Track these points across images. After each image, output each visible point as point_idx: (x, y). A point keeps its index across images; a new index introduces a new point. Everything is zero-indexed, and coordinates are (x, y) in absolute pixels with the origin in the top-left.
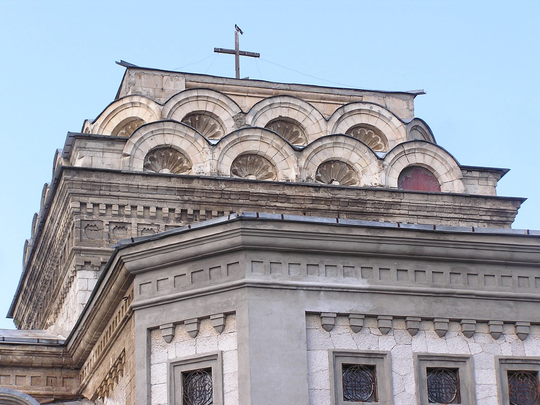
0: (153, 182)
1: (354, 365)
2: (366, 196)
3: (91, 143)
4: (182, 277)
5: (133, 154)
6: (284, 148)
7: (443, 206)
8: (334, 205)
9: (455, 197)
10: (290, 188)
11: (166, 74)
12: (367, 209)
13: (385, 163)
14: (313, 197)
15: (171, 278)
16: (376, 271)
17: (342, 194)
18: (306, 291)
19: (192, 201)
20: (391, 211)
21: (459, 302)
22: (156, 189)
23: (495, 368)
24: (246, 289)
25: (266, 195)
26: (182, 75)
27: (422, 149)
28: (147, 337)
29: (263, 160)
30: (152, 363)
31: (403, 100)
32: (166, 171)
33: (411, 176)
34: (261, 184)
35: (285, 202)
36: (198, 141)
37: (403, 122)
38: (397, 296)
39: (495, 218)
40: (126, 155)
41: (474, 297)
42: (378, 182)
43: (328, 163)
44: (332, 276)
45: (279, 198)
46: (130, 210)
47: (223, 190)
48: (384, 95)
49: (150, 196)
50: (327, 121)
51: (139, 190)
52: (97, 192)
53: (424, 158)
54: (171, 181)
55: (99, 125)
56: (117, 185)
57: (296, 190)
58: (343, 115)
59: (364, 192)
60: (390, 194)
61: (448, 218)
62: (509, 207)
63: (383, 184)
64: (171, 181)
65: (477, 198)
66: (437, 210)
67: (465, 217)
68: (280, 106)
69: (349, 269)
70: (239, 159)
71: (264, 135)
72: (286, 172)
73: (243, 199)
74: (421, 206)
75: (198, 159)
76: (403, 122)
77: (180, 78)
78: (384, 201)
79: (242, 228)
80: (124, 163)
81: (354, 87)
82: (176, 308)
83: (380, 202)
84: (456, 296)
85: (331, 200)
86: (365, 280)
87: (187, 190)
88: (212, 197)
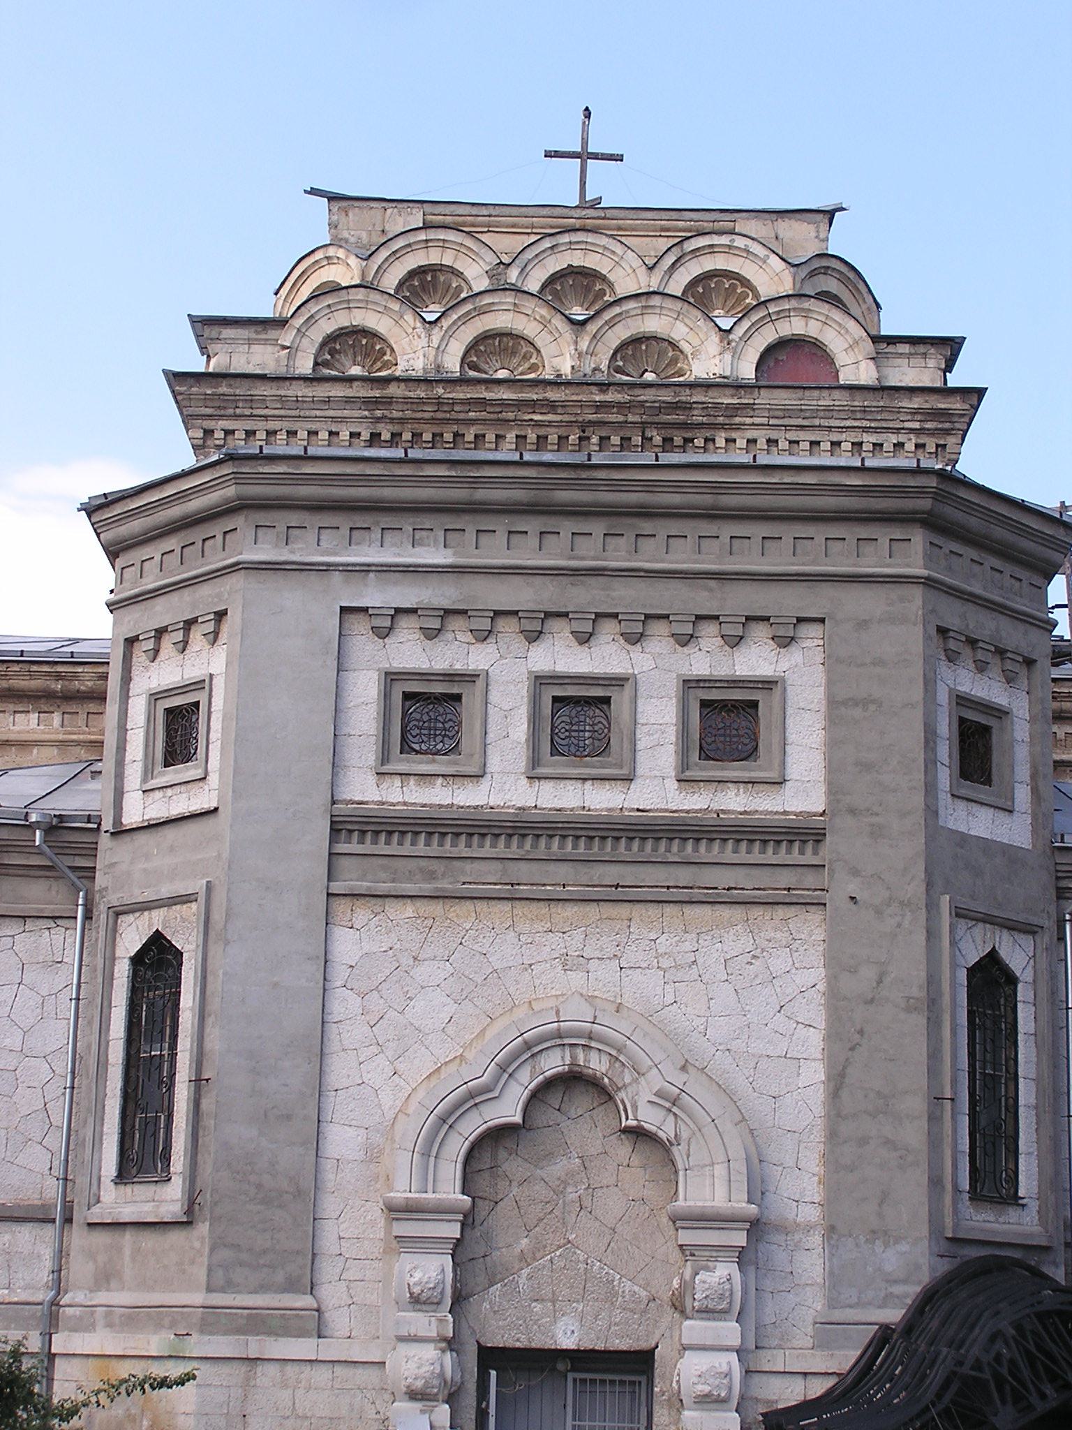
0: (323, 389)
1: (425, 693)
2: (690, 396)
3: (228, 330)
4: (171, 554)
5: (296, 345)
6: (553, 321)
7: (832, 408)
8: (634, 414)
9: (854, 391)
10: (555, 388)
11: (390, 205)
12: (694, 418)
13: (731, 337)
14: (596, 402)
15: (158, 558)
16: (470, 535)
17: (647, 395)
18: (344, 573)
19: (390, 419)
20: (737, 420)
21: (616, 583)
22: (328, 400)
23: (676, 696)
24: (243, 571)
25: (515, 402)
26: (419, 205)
27: (803, 310)
28: (124, 652)
29: (522, 342)
30: (131, 695)
31: (809, 223)
32: (356, 370)
33: (785, 358)
34: (505, 385)
35: (549, 413)
36: (405, 317)
37: (789, 263)
38: (503, 576)
39: (928, 425)
40: (285, 348)
41: (642, 574)
42: (718, 371)
43: (636, 341)
44: (395, 545)
45: (537, 406)
46: (285, 437)
47: (439, 397)
48: (774, 216)
49: (318, 413)
50: (651, 269)
51: (299, 405)
52: (230, 411)
53: (807, 325)
54: (351, 387)
55: (283, 298)
56: (261, 398)
57: (567, 391)
58: (681, 257)
59: (687, 390)
60: (735, 391)
61: (842, 428)
62: (956, 404)
63: (728, 373)
64: (351, 387)
65: (896, 391)
66: (821, 414)
67: (873, 425)
68: (570, 249)
69: (424, 533)
70: (479, 343)
71: (519, 300)
72: (556, 361)
73: (476, 412)
74: (792, 410)
75: (407, 347)
76: (789, 263)
77: (414, 211)
78: (723, 404)
79: (233, 473)
80: (278, 360)
81: (729, 205)
82: (160, 604)
83: (717, 406)
84: (609, 573)
85: (628, 405)
86: (449, 551)
87: (379, 400)
88: (422, 411)
